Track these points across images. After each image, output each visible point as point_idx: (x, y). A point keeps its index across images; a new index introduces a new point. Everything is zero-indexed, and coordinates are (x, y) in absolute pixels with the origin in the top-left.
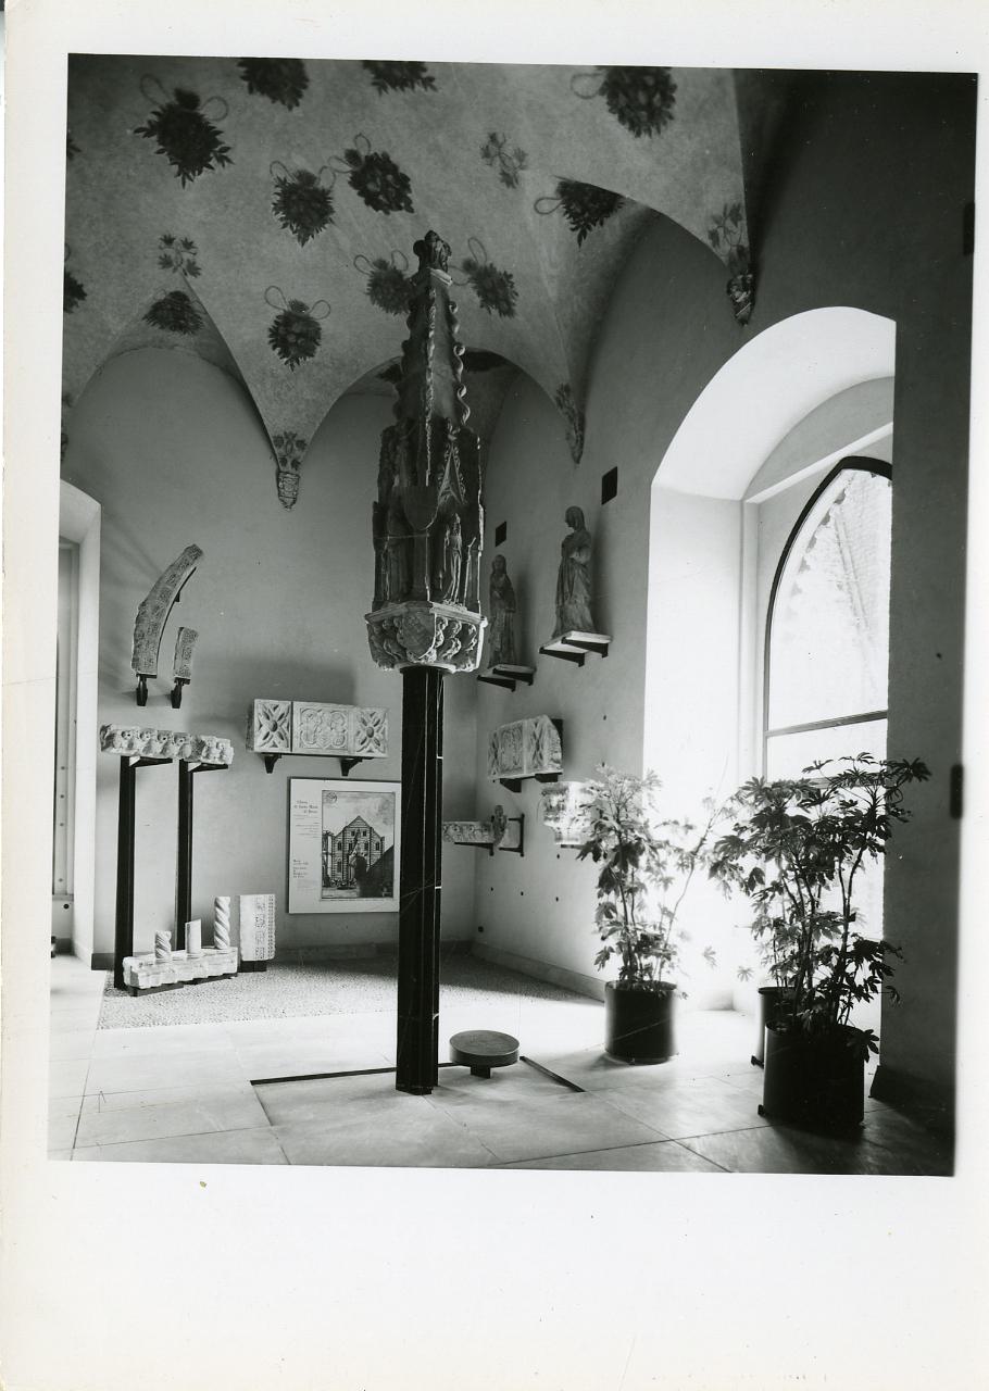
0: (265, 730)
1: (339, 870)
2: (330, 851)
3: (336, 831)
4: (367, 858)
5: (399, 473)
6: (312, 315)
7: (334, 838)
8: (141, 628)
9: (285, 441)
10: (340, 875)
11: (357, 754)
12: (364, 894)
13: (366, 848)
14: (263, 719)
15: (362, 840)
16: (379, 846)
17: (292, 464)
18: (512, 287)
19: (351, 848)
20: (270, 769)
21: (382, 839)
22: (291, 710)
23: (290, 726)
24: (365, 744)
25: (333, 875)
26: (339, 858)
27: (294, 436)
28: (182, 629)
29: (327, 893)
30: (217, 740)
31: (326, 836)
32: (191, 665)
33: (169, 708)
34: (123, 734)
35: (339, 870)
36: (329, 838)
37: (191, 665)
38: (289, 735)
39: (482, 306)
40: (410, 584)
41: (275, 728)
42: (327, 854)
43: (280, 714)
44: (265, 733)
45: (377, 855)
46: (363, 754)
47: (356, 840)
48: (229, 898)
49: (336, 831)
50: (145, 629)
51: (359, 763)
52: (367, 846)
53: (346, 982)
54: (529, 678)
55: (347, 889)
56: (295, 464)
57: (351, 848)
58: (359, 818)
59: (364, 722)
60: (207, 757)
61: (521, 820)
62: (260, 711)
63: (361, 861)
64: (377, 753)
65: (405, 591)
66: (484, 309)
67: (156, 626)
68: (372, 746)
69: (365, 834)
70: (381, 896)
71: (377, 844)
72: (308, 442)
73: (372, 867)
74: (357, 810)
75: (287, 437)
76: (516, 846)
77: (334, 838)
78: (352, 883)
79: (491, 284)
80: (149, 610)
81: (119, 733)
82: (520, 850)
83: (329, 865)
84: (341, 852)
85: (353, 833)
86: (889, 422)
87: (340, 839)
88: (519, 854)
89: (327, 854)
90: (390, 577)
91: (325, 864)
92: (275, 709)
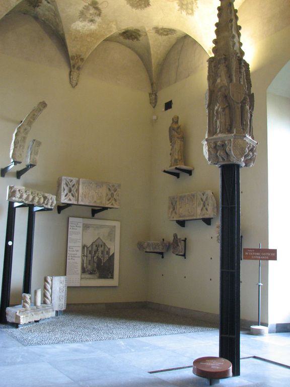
0: (66, 192)
2: (85, 255)
3: (89, 244)
5: (220, 76)
6: (99, 7)
7: (87, 248)
8: (17, 138)
9: (76, 58)
10: (89, 267)
11: (107, 206)
12: (101, 277)
13: (102, 254)
14: (65, 186)
15: (100, 249)
16: (108, 253)
17: (77, 69)
18: (196, 4)
19: (95, 253)
20: (59, 212)
21: (109, 249)
22: (78, 182)
23: (78, 190)
24: (110, 200)
25: (87, 267)
26: (89, 258)
27: (80, 56)
28: (34, 140)
29: (83, 276)
30: (52, 196)
31: (84, 247)
32: (37, 158)
33: (15, 179)
34: (19, 190)
35: (90, 253)
36: (85, 248)
37: (37, 158)
38: (77, 195)
39: (179, 10)
41: (70, 191)
43: (73, 184)
44: (65, 194)
45: (107, 257)
46: (109, 206)
47: (97, 249)
49: (89, 244)
50: (20, 139)
51: (106, 211)
52: (102, 253)
53: (128, 324)
54: (190, 172)
56: (79, 68)
57: (95, 253)
58: (99, 238)
59: (109, 189)
60: (47, 204)
61: (185, 240)
62: (64, 182)
63: (99, 260)
64: (116, 206)
65: (229, 129)
66: (180, 12)
67: (25, 138)
68: (113, 202)
69: (101, 246)
70: (108, 278)
71: (107, 252)
72: (85, 59)
73: (104, 263)
75: (77, 56)
76: (182, 254)
77: (87, 248)
79: (186, 2)
80: (22, 130)
81: (18, 190)
82: (184, 255)
83: (85, 262)
86: (259, 70)
87: (90, 249)
88: (183, 257)
89: (84, 256)
90: (220, 123)
91: (83, 261)
92: (71, 182)
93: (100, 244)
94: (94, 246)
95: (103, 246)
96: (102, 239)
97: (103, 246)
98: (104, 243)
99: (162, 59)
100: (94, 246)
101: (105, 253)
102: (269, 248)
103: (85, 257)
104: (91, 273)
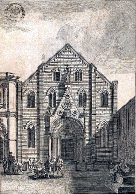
1: (31, 142)
2: (12, 108)
3: (26, 71)
4: (84, 121)
7: (19, 86)
10: (31, 154)
15: (74, 90)
16: (107, 98)
21: (113, 86)
35: (31, 142)
36: (12, 86)
40: (48, 127)
42: (16, 116)
45: (103, 116)
47: (63, 89)
48: (42, 169)
52: (82, 100)
55: (46, 177)
58: (67, 48)
69: (79, 76)
71: (104, 96)
74: (62, 33)
77: (19, 86)
78: (55, 167)
84: (32, 111)
85: (57, 76)
87: (32, 87)
93: (75, 66)
94: (48, 78)
95: (86, 77)
96: (79, 50)
97: (86, 77)
98: (91, 66)
99: (4, 181)
100: (48, 78)
101: (97, 100)
102: (5, 76)
103: (12, 120)
104: (39, 176)
